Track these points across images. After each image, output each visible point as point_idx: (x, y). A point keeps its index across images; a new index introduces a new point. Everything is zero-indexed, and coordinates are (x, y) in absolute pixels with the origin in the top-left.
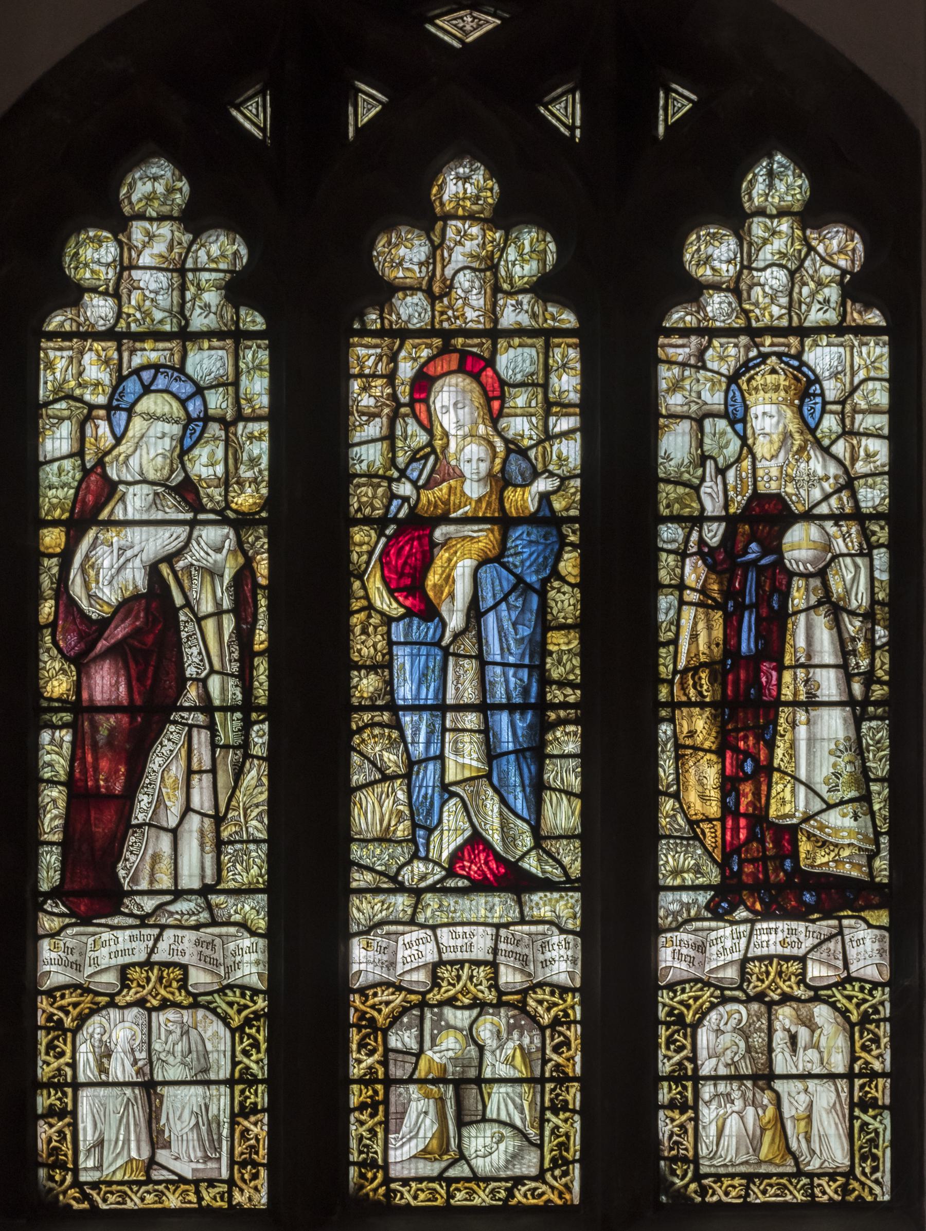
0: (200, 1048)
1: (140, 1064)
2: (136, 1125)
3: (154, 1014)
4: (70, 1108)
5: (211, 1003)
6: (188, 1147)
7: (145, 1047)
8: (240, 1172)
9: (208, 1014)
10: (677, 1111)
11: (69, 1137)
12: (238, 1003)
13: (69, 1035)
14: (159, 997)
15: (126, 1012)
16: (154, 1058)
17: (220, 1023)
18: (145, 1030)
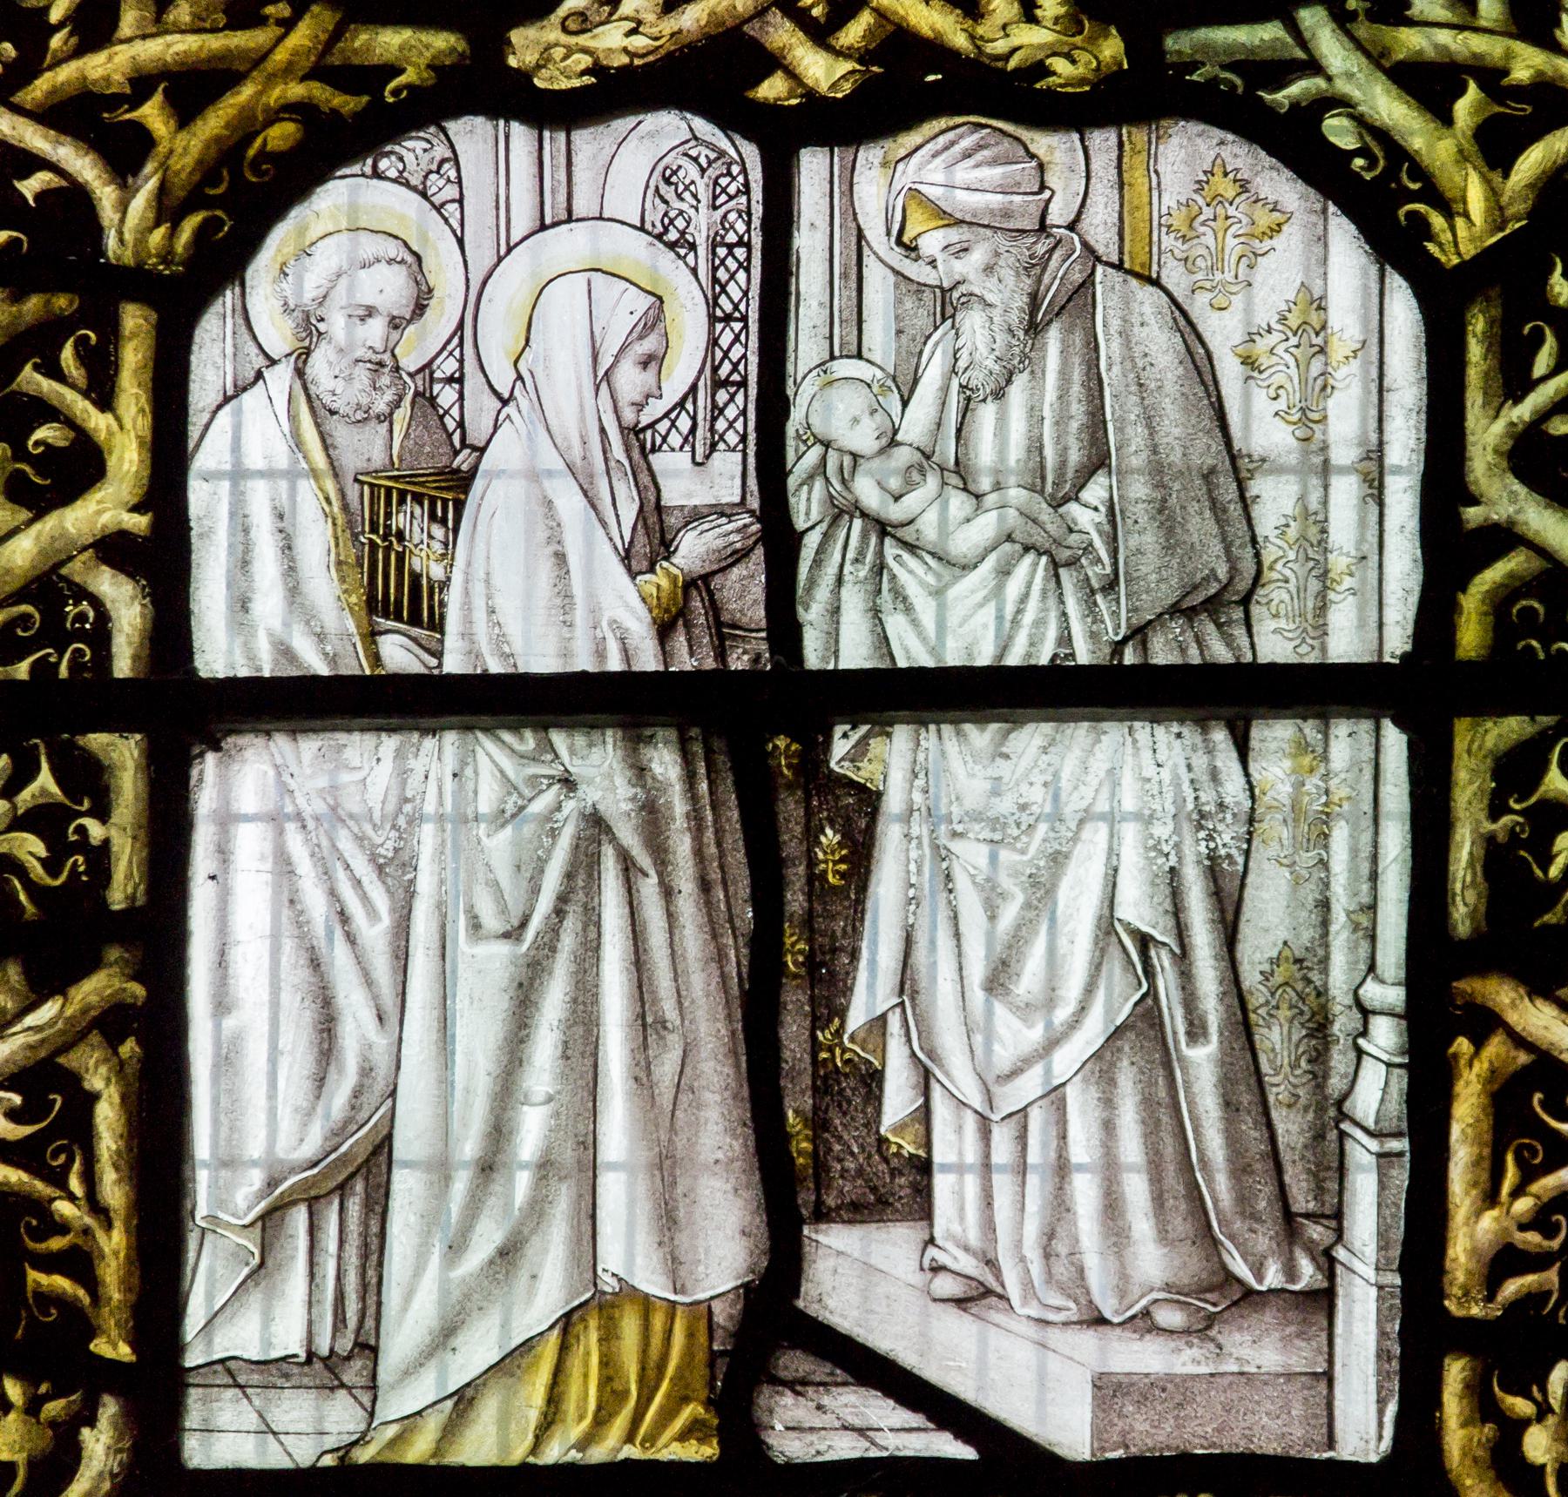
0: (1176, 424)
1: (693, 549)
2: (646, 1025)
3: (813, 166)
4: (125, 885)
5: (1278, 71)
6: (1060, 1205)
7: (740, 409)
8: (1483, 1407)
9: (1240, 155)
10: (1502, 837)
11: (108, 1117)
12: (1491, 77)
13: (134, 319)
14: (854, 33)
15: (589, 143)
16: (806, 507)
17: (1343, 235)
18: (744, 288)
